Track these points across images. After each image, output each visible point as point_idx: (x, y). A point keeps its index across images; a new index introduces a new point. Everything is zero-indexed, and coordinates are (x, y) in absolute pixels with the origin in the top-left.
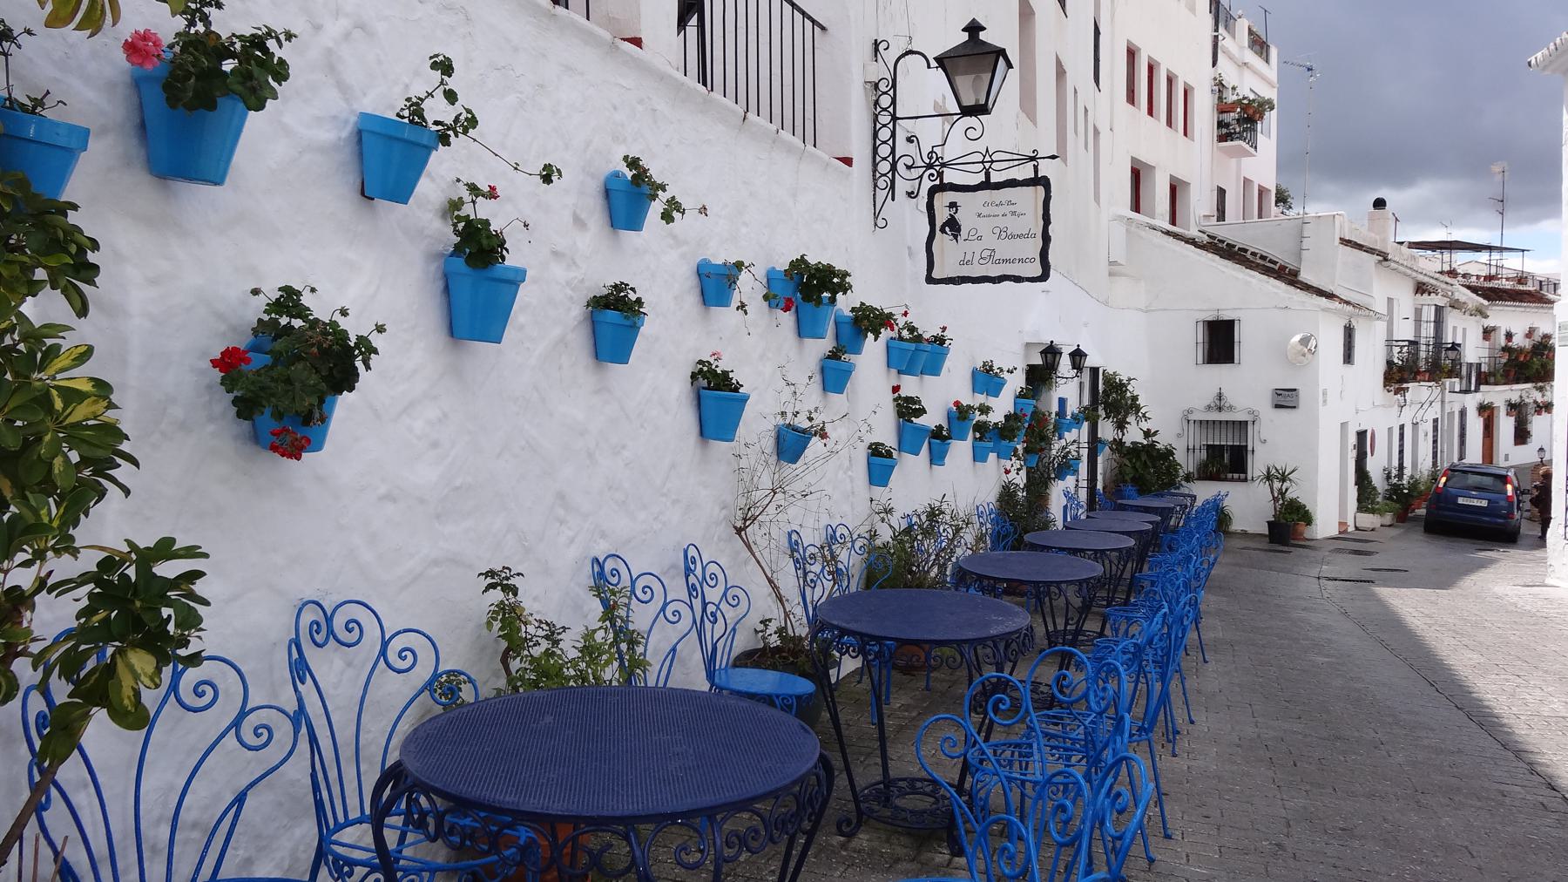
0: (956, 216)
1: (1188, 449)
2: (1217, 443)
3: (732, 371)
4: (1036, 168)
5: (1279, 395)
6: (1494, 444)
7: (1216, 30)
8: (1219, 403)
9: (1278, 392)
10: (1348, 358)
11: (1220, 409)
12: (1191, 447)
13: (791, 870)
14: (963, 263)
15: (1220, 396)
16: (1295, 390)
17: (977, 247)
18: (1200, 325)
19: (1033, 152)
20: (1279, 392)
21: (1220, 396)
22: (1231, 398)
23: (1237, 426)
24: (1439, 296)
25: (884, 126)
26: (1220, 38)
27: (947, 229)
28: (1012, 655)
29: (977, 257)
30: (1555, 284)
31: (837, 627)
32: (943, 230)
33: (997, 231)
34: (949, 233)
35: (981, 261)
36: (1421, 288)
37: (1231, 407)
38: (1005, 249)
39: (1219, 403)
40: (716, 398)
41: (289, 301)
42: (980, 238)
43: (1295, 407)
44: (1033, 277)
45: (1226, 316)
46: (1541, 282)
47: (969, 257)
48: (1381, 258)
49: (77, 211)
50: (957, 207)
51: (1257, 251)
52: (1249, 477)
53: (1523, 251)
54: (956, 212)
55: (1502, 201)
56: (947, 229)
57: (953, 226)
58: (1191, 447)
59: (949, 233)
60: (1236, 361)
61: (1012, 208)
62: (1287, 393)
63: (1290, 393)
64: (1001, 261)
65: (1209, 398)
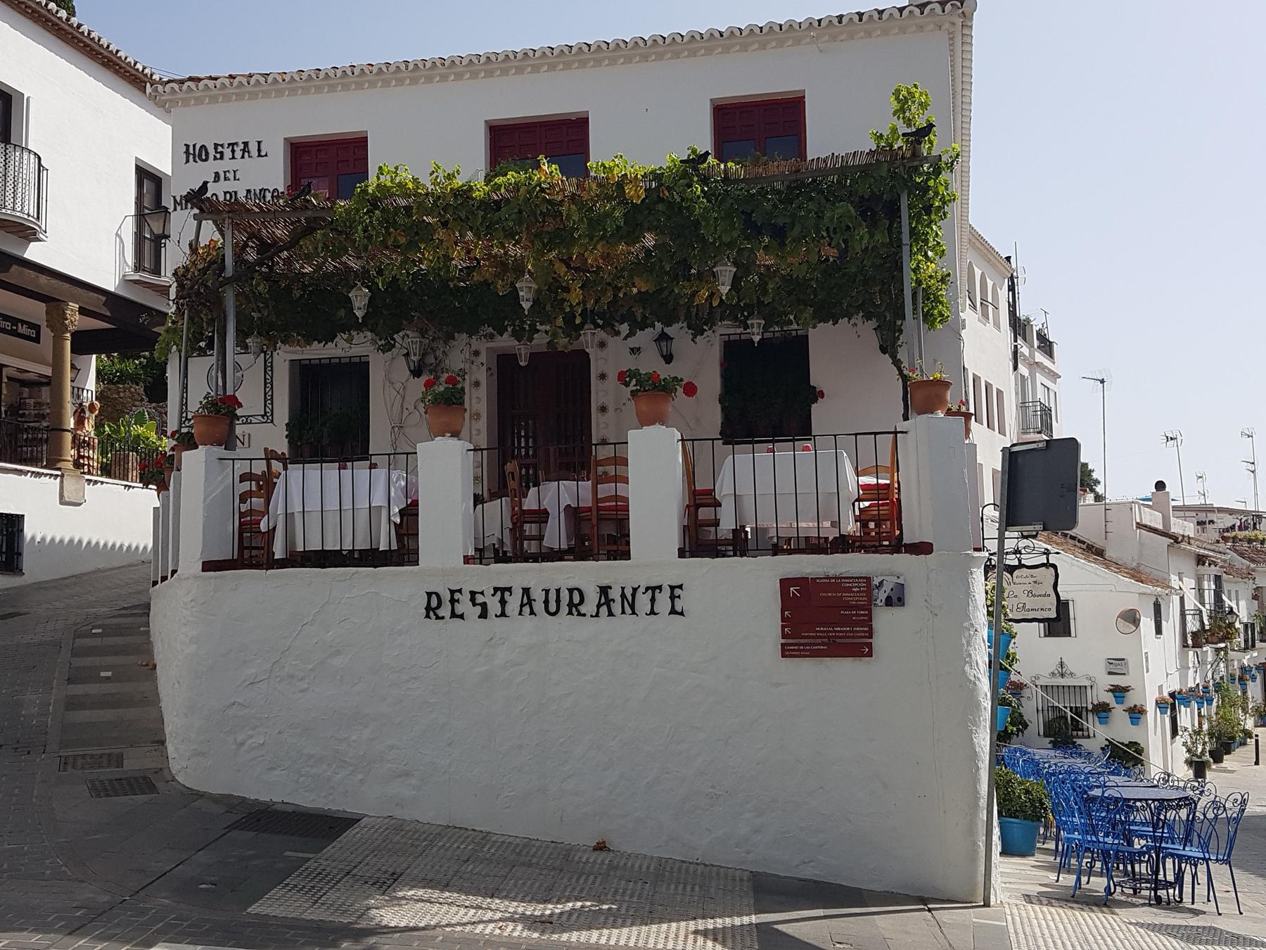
1: (1038, 710)
3: (482, 593)
4: (1048, 559)
6: (69, 50)
7: (1016, 341)
9: (1110, 661)
10: (1159, 630)
11: (1062, 675)
12: (1040, 708)
15: (1062, 664)
16: (1124, 659)
21: (1062, 664)
22: (1071, 666)
24: (1217, 568)
26: (1019, 346)
29: (1015, 607)
31: (1176, 799)
33: (1026, 592)
36: (1201, 560)
37: (1071, 674)
40: (216, 578)
41: (786, 652)
42: (1016, 596)
43: (1124, 674)
48: (1172, 541)
49: (860, 648)
52: (1092, 735)
55: (1253, 463)
58: (1040, 708)
60: (1073, 633)
61: (1033, 579)
62: (1117, 662)
65: (1053, 666)
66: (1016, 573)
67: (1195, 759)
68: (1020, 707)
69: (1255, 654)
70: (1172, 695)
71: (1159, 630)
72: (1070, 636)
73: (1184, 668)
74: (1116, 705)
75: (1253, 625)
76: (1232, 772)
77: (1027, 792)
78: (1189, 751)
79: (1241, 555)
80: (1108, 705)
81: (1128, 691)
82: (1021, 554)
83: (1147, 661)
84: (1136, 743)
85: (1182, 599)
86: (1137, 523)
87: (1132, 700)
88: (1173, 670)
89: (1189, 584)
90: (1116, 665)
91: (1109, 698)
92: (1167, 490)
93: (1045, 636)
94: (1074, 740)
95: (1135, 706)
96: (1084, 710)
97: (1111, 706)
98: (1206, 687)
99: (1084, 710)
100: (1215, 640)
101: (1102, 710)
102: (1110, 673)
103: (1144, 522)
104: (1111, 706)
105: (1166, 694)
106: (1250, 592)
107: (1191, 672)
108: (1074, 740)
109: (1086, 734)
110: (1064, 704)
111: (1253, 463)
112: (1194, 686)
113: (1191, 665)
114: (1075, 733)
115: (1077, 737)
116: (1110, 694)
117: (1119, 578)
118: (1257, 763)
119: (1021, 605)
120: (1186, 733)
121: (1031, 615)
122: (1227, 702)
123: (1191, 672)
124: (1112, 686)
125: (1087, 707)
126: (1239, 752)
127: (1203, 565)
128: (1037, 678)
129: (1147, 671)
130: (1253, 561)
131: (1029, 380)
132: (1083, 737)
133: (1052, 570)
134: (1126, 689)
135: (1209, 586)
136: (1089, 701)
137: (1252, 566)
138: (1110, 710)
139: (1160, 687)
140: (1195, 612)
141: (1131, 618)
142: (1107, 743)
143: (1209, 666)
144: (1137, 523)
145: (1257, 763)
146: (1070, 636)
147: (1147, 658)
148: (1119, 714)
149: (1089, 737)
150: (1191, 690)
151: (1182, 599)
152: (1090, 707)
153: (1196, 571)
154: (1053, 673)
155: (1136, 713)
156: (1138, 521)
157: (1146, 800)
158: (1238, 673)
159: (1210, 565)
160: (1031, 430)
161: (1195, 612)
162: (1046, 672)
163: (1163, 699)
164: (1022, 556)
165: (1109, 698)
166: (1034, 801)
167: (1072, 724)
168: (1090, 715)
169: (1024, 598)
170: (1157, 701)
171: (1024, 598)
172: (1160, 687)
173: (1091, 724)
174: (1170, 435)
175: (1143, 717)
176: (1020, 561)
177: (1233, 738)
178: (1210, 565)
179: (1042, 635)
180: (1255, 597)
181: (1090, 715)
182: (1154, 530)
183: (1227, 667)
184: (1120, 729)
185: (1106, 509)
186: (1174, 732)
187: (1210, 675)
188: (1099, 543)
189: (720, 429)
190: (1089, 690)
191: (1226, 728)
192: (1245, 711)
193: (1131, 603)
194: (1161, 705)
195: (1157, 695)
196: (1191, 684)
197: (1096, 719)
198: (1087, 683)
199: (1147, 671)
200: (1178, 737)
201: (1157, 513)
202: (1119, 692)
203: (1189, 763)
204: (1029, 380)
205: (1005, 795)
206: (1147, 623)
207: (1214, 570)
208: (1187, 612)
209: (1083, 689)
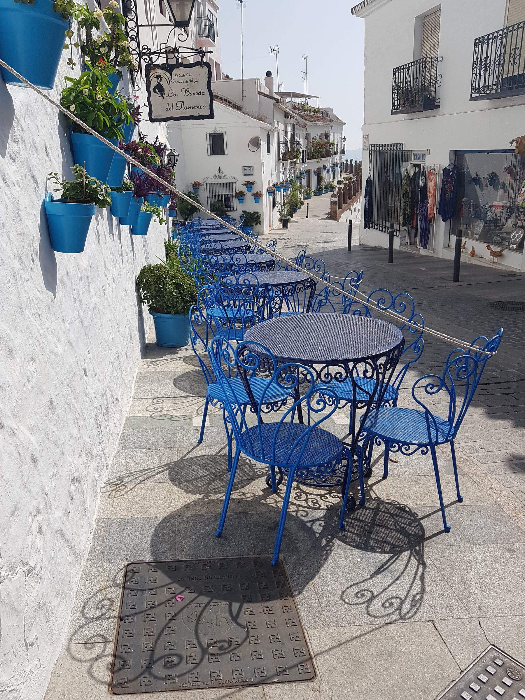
0: (161, 83)
2: (220, 194)
5: (245, 169)
8: (220, 174)
10: (269, 151)
11: (220, 177)
12: (209, 196)
13: (464, 410)
14: (168, 109)
15: (220, 171)
16: (252, 166)
17: (173, 100)
18: (208, 135)
19: (200, 49)
20: (245, 168)
21: (220, 171)
22: (225, 172)
23: (228, 185)
25: (132, 30)
27: (157, 90)
28: (273, 304)
29: (175, 106)
30: (327, 113)
32: (155, 91)
34: (159, 93)
35: (177, 108)
37: (225, 176)
38: (188, 101)
39: (220, 174)
42: (175, 95)
43: (252, 175)
44: (203, 119)
45: (220, 131)
46: (322, 112)
47: (170, 106)
48: (276, 102)
50: (161, 78)
51: (222, 97)
52: (235, 209)
53: (317, 97)
54: (161, 80)
55: (306, 73)
56: (157, 90)
57: (160, 89)
58: (209, 196)
59: (159, 93)
60: (226, 153)
62: (248, 168)
63: (250, 168)
64: (188, 108)
65: (215, 172)
66: (175, 72)
67: (284, 218)
68: (198, 196)
69: (306, 165)
70: (274, 185)
71: (269, 151)
72: (224, 154)
73: (278, 172)
74: (248, 193)
75: (306, 151)
76: (297, 222)
77: (178, 286)
78: (281, 214)
79: (301, 117)
80: (244, 192)
81: (254, 184)
82: (179, 53)
83: (263, 167)
84: (257, 212)
85: (278, 133)
86: (258, 91)
87: (256, 189)
88: (274, 173)
89: (282, 127)
90: (248, 170)
91: (244, 189)
92: (272, 76)
93: (211, 155)
94: (226, 213)
95: (257, 192)
96: (231, 196)
97: (245, 193)
98: (287, 182)
99: (231, 196)
100: (291, 157)
101: (240, 195)
102: (245, 175)
103: (262, 91)
104: (245, 193)
105: (271, 185)
106: (305, 135)
107: (281, 174)
108: (226, 213)
109: (232, 209)
110: (223, 192)
111: (306, 73)
112: (282, 181)
113: (281, 170)
114: (226, 209)
115: (228, 211)
116: (245, 186)
117: (250, 119)
118: (307, 217)
119: (179, 104)
120: (280, 205)
121: (188, 113)
122: (294, 189)
123: (281, 174)
124: (246, 182)
125: (233, 194)
126: (298, 212)
127: (288, 118)
128: (207, 179)
129: (264, 173)
130: (306, 120)
131: (202, 5)
132: (231, 211)
133: (205, 68)
134: (252, 183)
135: (289, 129)
136: (234, 191)
137: (306, 122)
138: (244, 195)
139: (269, 181)
140: (284, 142)
141: (255, 143)
142: (243, 213)
143: (288, 171)
144: (258, 91)
145: (307, 217)
146: (224, 154)
147: (263, 165)
148: (249, 197)
149: (233, 210)
150: (281, 183)
151: (278, 133)
152: (234, 194)
153: (285, 121)
154: (215, 176)
155: (258, 196)
156: (259, 90)
157: (345, 362)
158: (298, 174)
159: (291, 118)
160: (204, 35)
161: (284, 142)
162: (211, 176)
163: (271, 188)
164: (180, 55)
165: (244, 189)
166: (185, 296)
167: (225, 204)
168: (234, 199)
169: (182, 97)
170: (267, 189)
171: (182, 97)
172: (269, 181)
173: (235, 203)
174: (273, 48)
175: (261, 198)
176: (177, 60)
177: (296, 206)
178: (291, 118)
179: (209, 154)
180: (306, 138)
181: (234, 199)
182: (266, 96)
183: (295, 171)
184: (250, 206)
185: (243, 83)
186: (274, 205)
187: (288, 176)
188: (239, 104)
189: (247, 211)
190: (234, 184)
191: (293, 201)
192: (301, 192)
193: (256, 133)
194: (270, 191)
195: (267, 186)
196: (281, 180)
197: (237, 200)
198: (233, 181)
199: (264, 173)
200: (276, 207)
201: (267, 89)
202: (249, 185)
203: (281, 220)
204: (202, 5)
205: (157, 292)
206: (264, 145)
207: (293, 121)
208: (281, 142)
209: (231, 185)
